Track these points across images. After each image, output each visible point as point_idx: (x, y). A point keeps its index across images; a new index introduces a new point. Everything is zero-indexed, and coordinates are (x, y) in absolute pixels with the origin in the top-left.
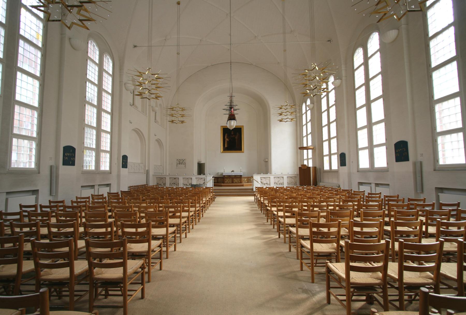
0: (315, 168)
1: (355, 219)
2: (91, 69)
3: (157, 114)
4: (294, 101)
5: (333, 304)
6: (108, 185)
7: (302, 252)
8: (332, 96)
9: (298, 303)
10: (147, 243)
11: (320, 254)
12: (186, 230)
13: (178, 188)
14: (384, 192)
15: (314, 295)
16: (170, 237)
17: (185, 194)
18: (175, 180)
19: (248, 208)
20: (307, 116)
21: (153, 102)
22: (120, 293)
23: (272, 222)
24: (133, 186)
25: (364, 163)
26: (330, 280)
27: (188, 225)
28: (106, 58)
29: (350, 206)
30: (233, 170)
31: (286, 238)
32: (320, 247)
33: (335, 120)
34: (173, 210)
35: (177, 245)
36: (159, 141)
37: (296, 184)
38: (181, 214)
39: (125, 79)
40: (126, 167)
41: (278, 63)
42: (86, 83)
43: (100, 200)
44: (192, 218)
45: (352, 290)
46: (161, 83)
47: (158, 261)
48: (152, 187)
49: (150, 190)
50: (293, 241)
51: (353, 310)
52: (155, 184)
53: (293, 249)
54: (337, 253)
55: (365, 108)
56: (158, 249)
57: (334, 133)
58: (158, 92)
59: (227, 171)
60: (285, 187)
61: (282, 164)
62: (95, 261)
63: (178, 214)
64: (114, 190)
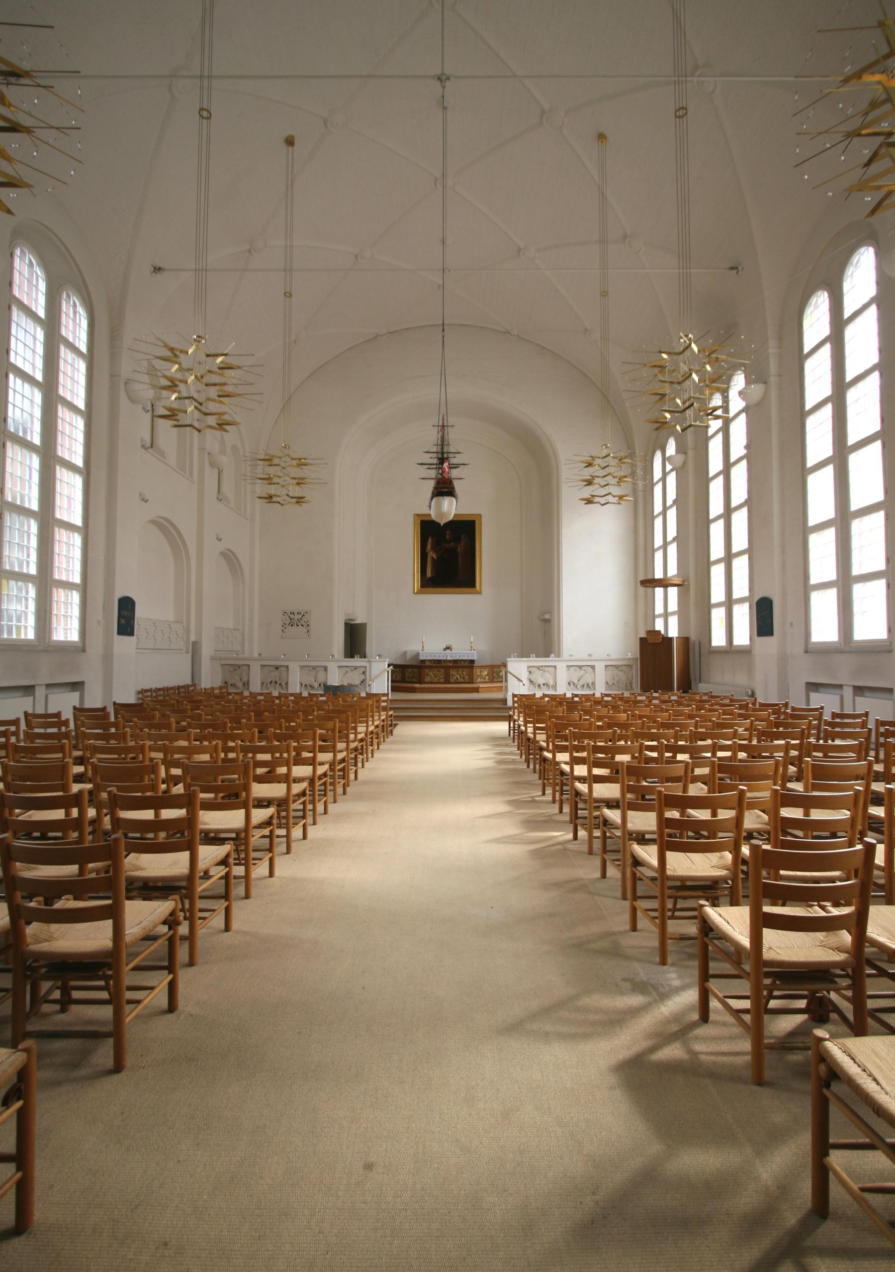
0: (685, 641)
1: (790, 785)
2: (21, 335)
3: (225, 474)
4: (630, 444)
5: (716, 1023)
6: (77, 686)
7: (635, 878)
8: (739, 430)
9: (617, 1020)
10: (187, 854)
11: (688, 883)
12: (304, 817)
13: (286, 696)
14: (878, 710)
15: (663, 996)
16: (257, 838)
17: (306, 714)
18: (277, 673)
19: (490, 754)
20: (666, 490)
21: (212, 439)
22: (104, 995)
23: (557, 794)
24: (150, 690)
25: (824, 628)
26: (710, 955)
27: (313, 802)
28: (68, 301)
29: (778, 748)
30: (448, 643)
31: (595, 840)
32: (685, 865)
33: (746, 503)
34: (267, 757)
35: (278, 861)
36: (229, 557)
37: (629, 686)
38: (289, 770)
39: (126, 368)
40: (131, 634)
41: (586, 330)
42: (7, 376)
43: (50, 730)
44: (325, 784)
45: (767, 981)
46: (235, 381)
47: (222, 904)
48: (209, 693)
49: (200, 701)
50: (612, 846)
51: (770, 1038)
52: (218, 683)
53: (613, 872)
54: (734, 879)
55: (829, 470)
56: (218, 872)
57: (740, 541)
58: (228, 408)
59: (431, 645)
60: (598, 695)
61: (593, 627)
62: (32, 904)
63: (283, 770)
64: (94, 700)
